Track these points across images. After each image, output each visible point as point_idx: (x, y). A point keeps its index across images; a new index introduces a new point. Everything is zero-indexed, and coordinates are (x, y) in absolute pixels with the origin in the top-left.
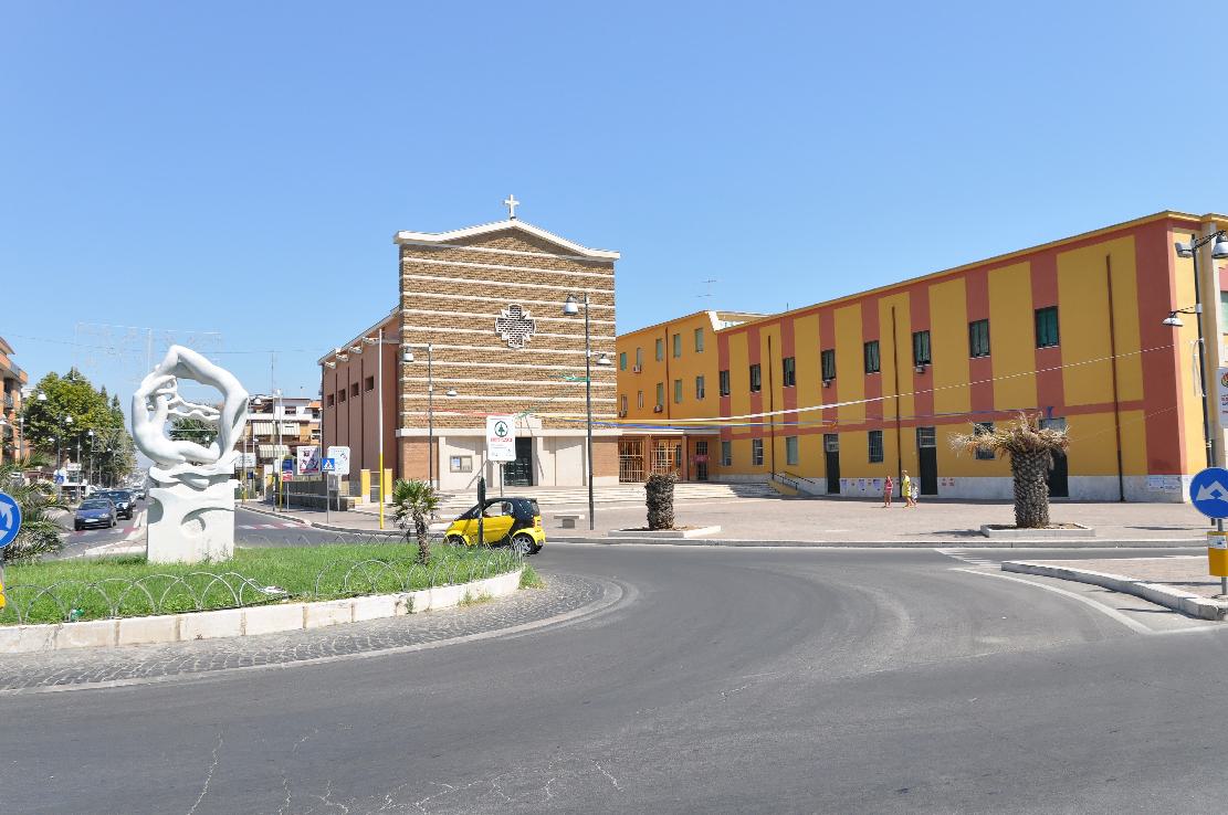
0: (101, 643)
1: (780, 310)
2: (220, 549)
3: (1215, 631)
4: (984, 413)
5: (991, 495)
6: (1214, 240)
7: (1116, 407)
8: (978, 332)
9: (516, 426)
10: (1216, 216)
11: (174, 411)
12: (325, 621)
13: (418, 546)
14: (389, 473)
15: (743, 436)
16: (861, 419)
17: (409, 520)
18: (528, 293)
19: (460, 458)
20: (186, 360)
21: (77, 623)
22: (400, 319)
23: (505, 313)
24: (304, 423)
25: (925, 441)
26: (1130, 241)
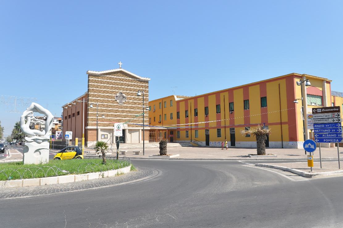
0: (18, 186)
1: (194, 95)
2: (45, 160)
3: (310, 180)
4: (247, 125)
5: (249, 146)
6: (305, 82)
7: (281, 123)
8: (246, 103)
9: (123, 126)
10: (296, 74)
11: (32, 121)
12: (80, 180)
13: (102, 160)
14: (83, 139)
15: (183, 130)
16: (204, 126)
17: (100, 151)
18: (123, 89)
19: (104, 135)
20: (36, 107)
21: (11, 180)
22: (87, 95)
23: (118, 94)
24: (56, 124)
25: (232, 132)
26: (284, 80)
